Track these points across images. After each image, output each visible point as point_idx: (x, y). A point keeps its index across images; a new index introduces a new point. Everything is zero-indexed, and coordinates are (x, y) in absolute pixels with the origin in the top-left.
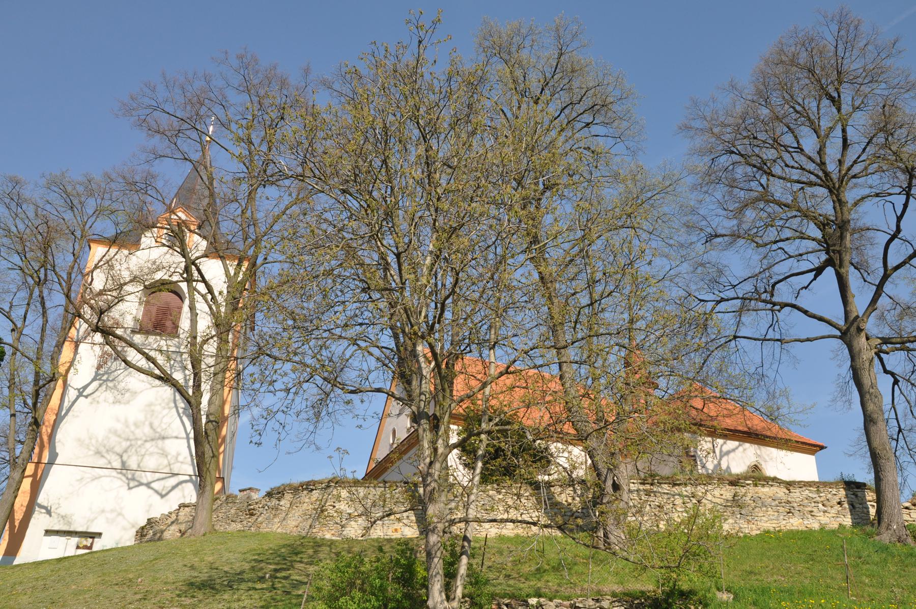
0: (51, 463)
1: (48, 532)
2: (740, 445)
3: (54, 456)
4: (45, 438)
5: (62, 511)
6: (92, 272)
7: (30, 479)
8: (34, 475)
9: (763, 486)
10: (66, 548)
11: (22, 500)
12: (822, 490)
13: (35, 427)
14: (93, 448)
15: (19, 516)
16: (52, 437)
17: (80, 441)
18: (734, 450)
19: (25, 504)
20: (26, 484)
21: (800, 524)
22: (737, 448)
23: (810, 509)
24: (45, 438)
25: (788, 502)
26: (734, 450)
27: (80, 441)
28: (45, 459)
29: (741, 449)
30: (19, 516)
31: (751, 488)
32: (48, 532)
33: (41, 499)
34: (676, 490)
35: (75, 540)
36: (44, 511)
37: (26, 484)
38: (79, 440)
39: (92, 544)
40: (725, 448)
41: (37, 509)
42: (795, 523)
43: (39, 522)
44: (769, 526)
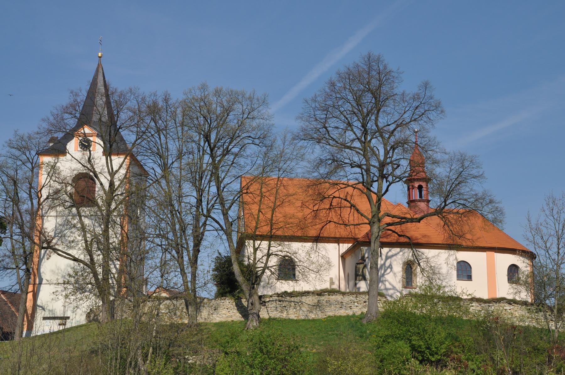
0: (40, 283)
1: (45, 318)
2: (401, 251)
3: (41, 280)
4: (36, 271)
5: (50, 308)
6: (41, 191)
7: (32, 293)
8: (33, 291)
9: (332, 295)
10: (55, 326)
11: (29, 304)
12: (358, 296)
13: (28, 273)
14: (60, 275)
15: (30, 312)
16: (38, 269)
17: (52, 271)
18: (396, 255)
19: (32, 305)
20: (30, 296)
21: (345, 312)
22: (398, 253)
23: (350, 305)
24: (36, 271)
25: (342, 302)
26: (396, 255)
27: (52, 271)
28: (37, 282)
29: (401, 253)
30: (30, 312)
31: (327, 296)
32: (45, 318)
33: (39, 302)
34: (292, 299)
35: (58, 321)
36: (41, 308)
37: (30, 296)
38: (53, 271)
39: (65, 322)
40: (390, 254)
41: (38, 308)
42: (342, 312)
43: (40, 314)
44: (331, 314)
